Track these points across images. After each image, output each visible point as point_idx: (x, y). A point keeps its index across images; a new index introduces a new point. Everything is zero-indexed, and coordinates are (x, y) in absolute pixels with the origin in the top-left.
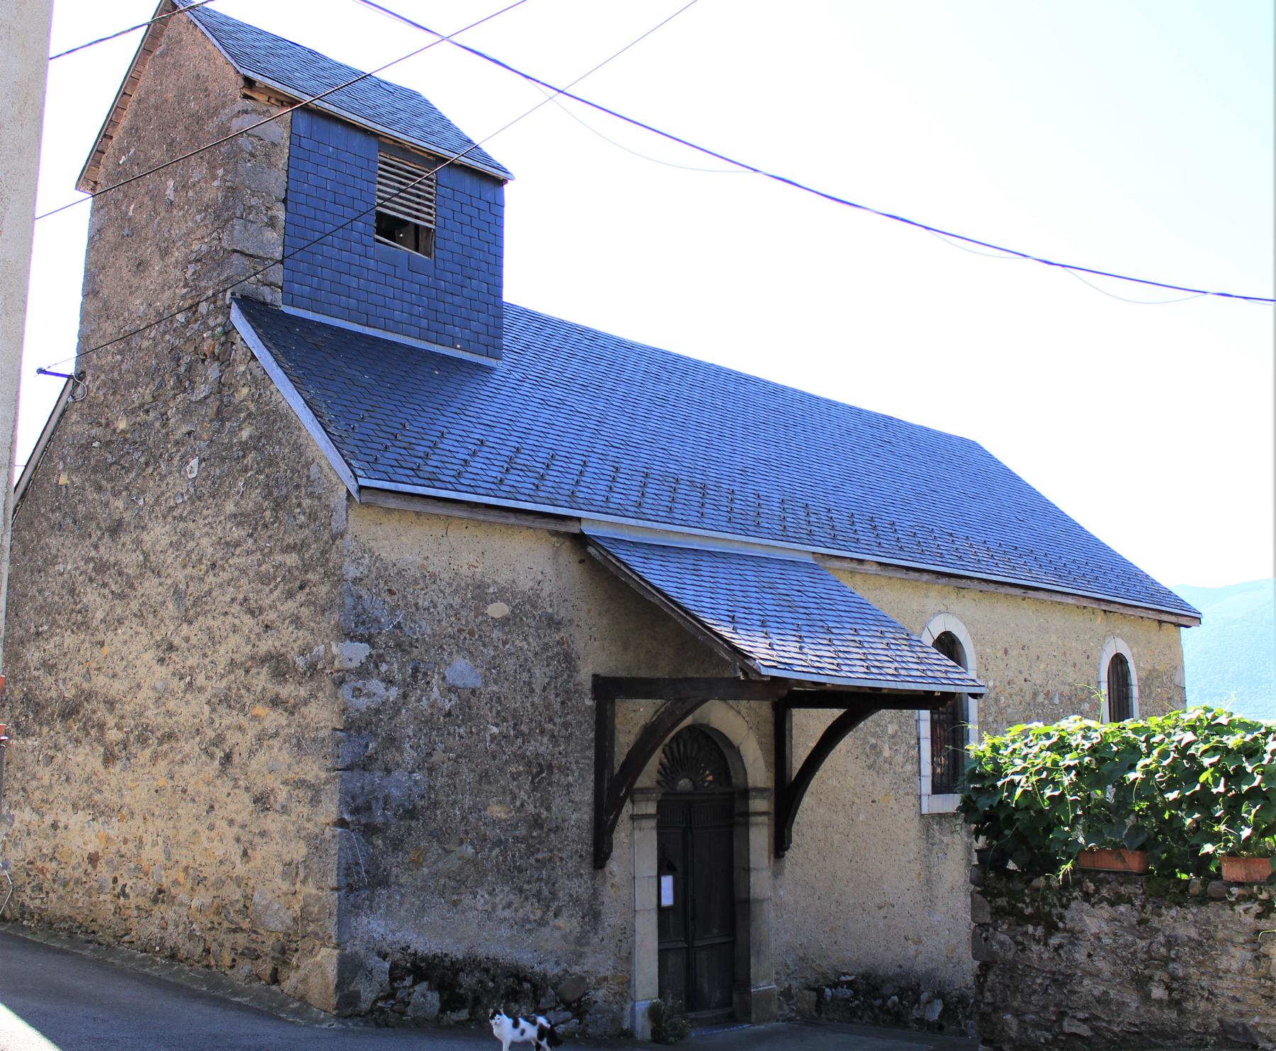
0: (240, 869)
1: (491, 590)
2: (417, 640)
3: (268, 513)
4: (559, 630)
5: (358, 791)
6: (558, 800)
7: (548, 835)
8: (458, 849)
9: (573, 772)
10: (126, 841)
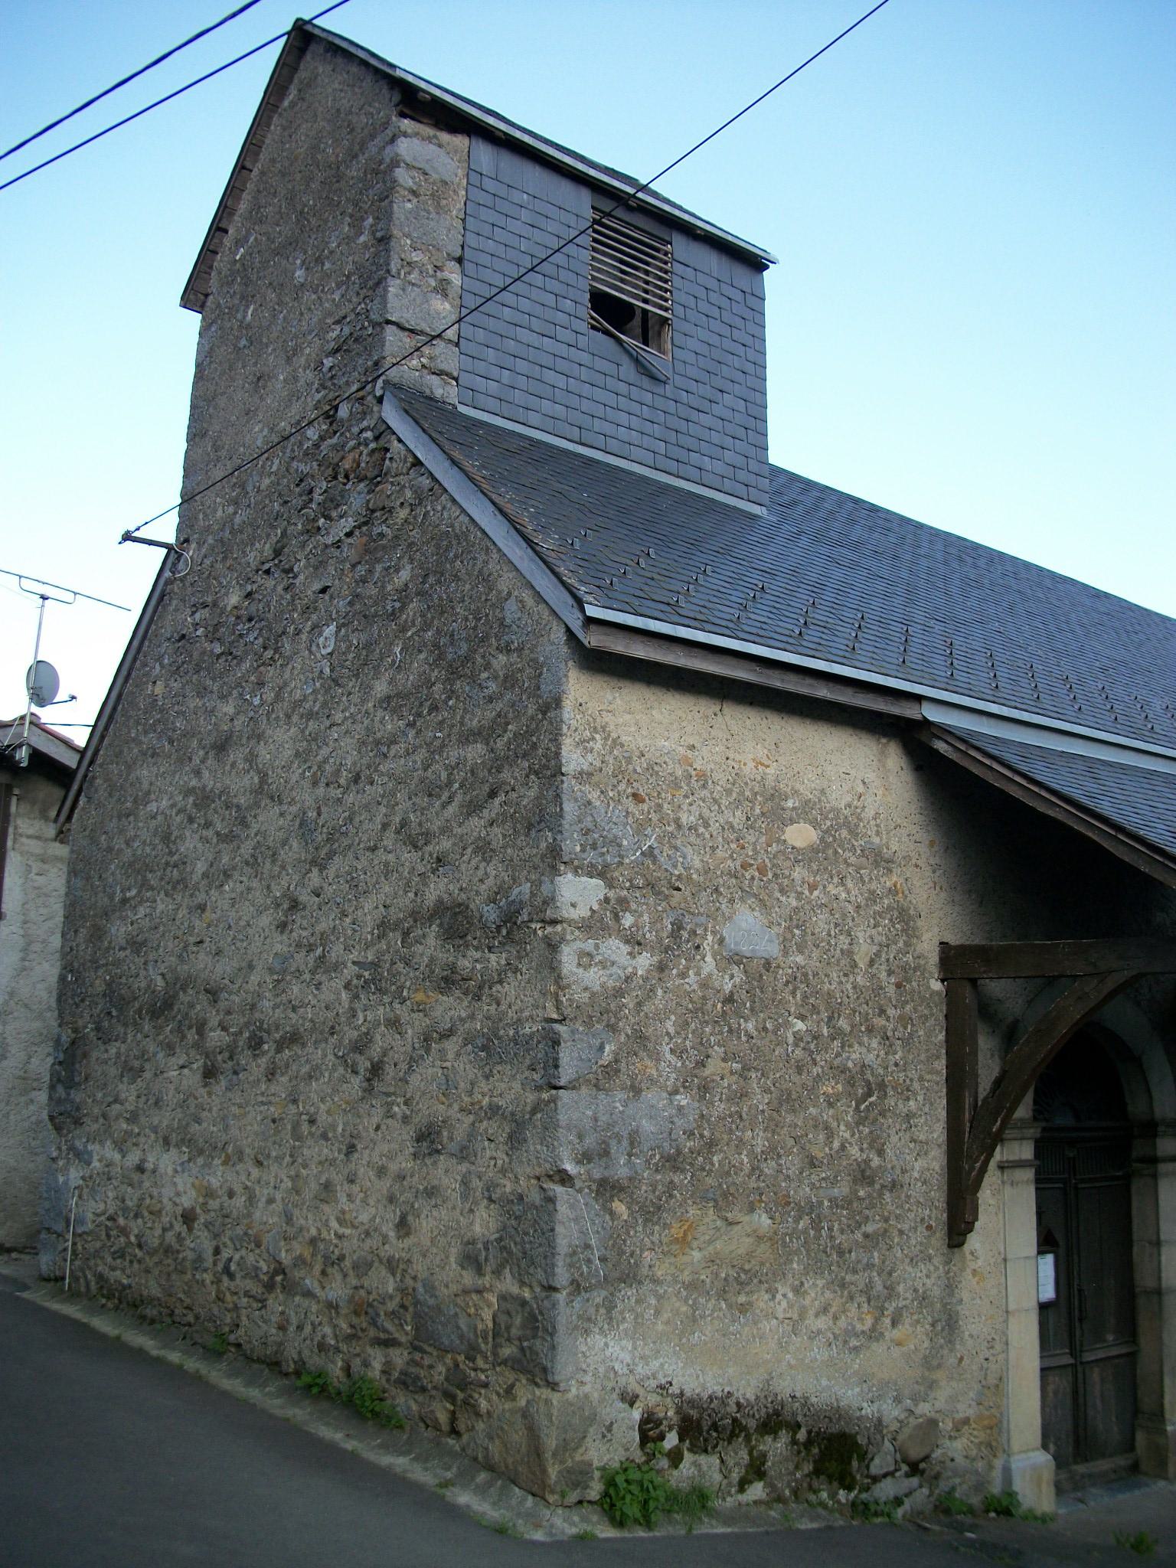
0: (396, 1247)
1: (790, 804)
2: (679, 877)
3: (438, 687)
4: (890, 871)
5: (588, 1124)
6: (894, 1139)
7: (881, 1195)
8: (746, 1218)
9: (915, 1094)
10: (231, 1194)
